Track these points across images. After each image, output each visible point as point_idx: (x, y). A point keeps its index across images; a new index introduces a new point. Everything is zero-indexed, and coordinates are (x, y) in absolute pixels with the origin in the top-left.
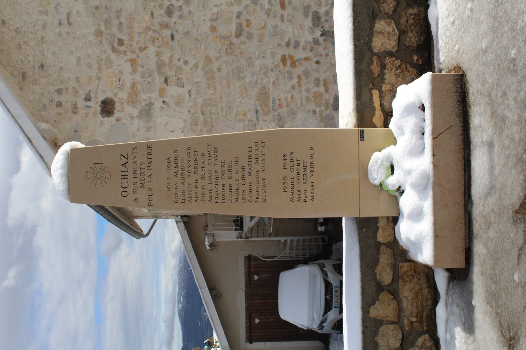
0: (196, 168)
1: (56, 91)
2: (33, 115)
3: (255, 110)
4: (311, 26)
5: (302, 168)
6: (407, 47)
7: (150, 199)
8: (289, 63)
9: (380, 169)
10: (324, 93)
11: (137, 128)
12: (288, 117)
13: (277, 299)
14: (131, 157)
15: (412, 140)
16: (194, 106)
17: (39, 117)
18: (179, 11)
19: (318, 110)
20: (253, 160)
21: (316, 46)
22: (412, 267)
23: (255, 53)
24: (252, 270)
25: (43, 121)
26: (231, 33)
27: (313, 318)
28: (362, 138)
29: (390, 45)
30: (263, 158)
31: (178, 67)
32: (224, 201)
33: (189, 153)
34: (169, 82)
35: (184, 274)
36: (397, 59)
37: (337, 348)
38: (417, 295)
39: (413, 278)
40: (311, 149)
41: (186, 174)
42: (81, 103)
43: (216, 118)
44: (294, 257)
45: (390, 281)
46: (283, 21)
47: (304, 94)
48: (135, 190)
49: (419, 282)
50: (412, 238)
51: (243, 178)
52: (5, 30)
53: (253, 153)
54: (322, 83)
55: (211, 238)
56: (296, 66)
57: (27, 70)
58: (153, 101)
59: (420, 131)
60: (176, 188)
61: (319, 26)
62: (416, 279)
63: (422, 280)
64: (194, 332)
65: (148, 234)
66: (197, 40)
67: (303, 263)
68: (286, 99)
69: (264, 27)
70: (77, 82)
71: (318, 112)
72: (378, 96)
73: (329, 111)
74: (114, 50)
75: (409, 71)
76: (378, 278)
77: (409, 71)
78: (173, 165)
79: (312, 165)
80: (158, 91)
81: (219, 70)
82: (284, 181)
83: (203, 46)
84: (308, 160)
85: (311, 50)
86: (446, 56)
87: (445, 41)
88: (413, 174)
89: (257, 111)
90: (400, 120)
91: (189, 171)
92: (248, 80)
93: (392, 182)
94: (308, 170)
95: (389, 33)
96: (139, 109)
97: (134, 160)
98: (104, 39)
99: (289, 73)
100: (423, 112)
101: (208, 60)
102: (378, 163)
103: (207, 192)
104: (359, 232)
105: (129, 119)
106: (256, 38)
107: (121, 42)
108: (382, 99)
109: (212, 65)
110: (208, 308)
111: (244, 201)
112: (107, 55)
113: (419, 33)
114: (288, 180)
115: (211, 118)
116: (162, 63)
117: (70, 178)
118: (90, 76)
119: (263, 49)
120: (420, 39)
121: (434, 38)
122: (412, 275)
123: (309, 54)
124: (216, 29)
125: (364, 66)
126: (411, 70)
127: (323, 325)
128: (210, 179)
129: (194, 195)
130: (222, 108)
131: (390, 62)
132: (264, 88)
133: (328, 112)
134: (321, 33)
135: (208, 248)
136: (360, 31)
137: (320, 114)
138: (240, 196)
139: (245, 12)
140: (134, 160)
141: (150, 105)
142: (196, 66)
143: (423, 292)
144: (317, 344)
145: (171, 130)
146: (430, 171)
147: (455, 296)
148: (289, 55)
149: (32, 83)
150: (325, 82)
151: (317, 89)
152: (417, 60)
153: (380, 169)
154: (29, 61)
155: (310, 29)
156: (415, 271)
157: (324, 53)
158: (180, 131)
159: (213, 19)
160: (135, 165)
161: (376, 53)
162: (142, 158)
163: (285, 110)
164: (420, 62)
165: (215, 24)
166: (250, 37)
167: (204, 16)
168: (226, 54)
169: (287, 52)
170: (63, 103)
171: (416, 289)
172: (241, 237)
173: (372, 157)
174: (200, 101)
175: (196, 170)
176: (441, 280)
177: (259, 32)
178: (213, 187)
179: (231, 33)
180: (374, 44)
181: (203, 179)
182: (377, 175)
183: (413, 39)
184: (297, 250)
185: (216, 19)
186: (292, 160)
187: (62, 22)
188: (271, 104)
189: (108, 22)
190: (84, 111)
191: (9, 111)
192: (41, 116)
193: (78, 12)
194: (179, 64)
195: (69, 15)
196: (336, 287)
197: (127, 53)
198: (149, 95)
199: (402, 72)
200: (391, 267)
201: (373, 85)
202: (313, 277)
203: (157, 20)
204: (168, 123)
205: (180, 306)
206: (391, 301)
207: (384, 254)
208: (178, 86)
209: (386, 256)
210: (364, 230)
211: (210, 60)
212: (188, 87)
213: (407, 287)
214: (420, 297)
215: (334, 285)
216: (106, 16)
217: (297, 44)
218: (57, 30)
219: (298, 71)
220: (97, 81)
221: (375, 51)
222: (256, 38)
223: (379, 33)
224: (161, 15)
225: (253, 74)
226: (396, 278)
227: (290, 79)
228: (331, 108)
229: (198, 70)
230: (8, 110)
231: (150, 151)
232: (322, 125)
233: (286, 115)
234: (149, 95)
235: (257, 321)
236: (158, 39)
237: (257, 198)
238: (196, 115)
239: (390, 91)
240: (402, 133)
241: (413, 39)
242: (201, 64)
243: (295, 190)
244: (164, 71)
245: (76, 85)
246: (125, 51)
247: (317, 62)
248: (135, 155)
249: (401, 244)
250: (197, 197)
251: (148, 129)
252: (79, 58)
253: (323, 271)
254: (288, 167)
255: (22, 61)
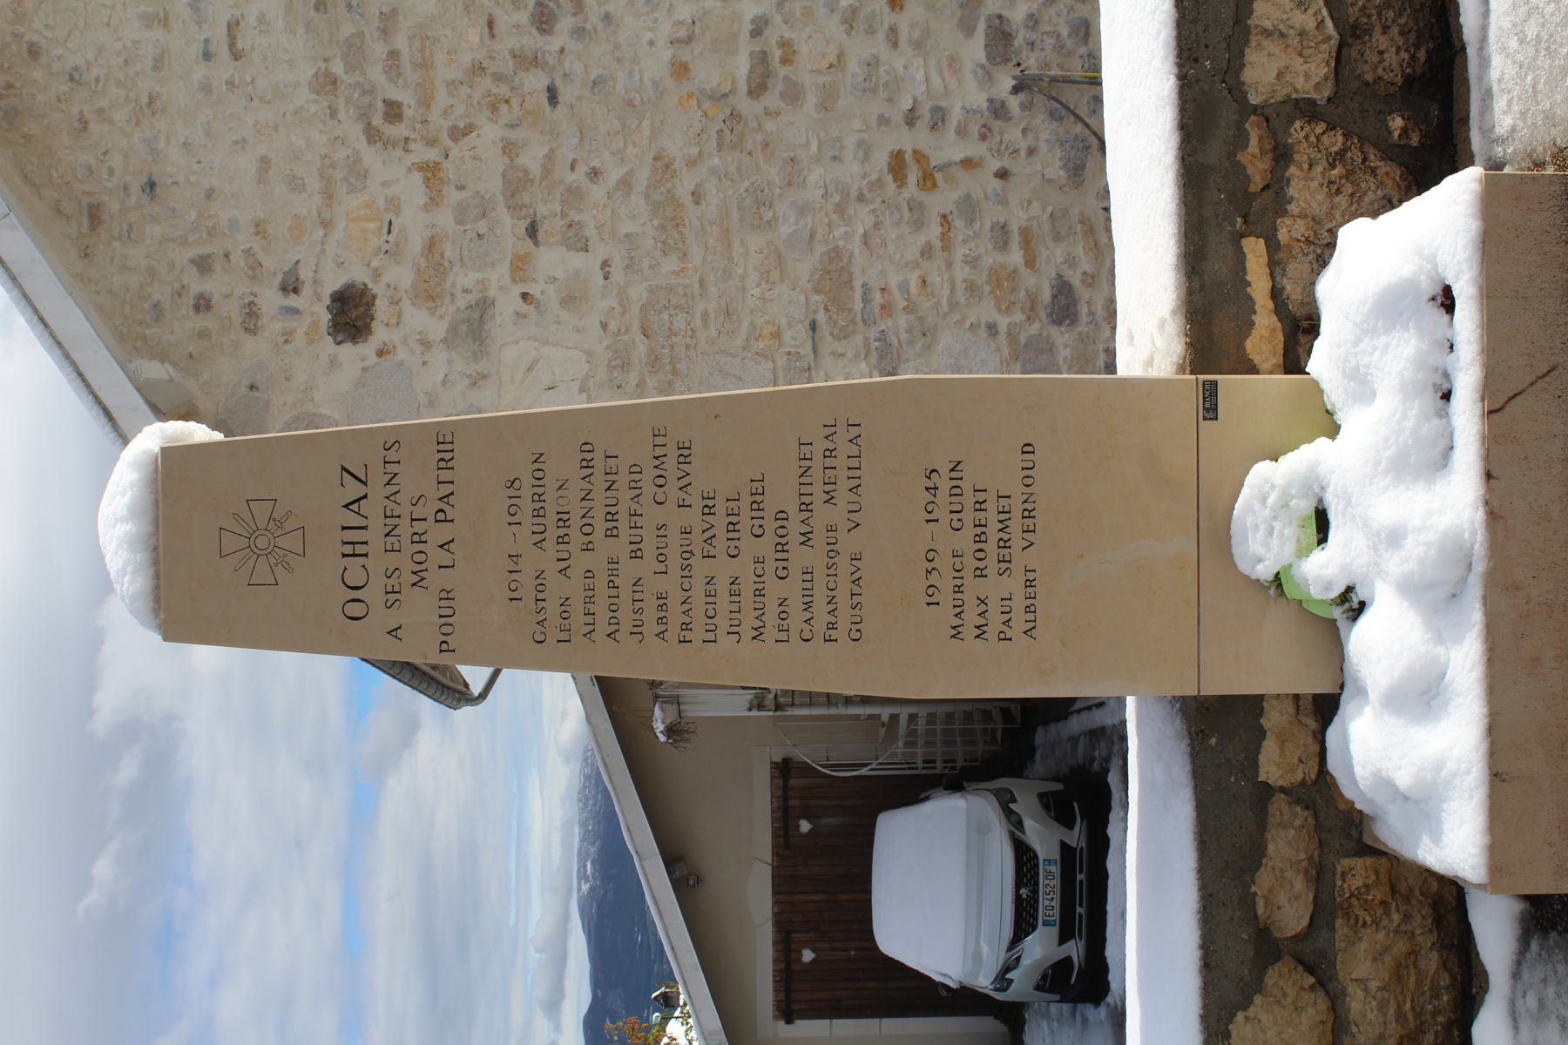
0: (611, 517)
1: (193, 261)
2: (122, 337)
3: (807, 324)
4: (984, 61)
5: (992, 517)
6: (1367, 84)
7: (446, 629)
8: (913, 176)
9: (1277, 525)
10: (1022, 269)
11: (441, 376)
12: (911, 343)
13: (870, 892)
14: (377, 478)
15: (1404, 417)
16: (618, 309)
17: (139, 344)
18: (575, 14)
19: (1003, 322)
20: (818, 490)
21: (997, 125)
22: (1382, 872)
23: (808, 144)
24: (792, 803)
25: (152, 357)
26: (733, 82)
27: (977, 956)
28: (1210, 404)
29: (1307, 76)
30: (856, 482)
31: (568, 190)
32: (711, 636)
33: (587, 465)
34: (540, 235)
35: (595, 796)
36: (1331, 127)
37: (1048, 1040)
38: (1398, 973)
39: (1387, 913)
40: (1027, 449)
41: (576, 539)
42: (270, 299)
43: (688, 347)
44: (920, 765)
45: (1305, 922)
46: (895, 44)
47: (961, 273)
48: (393, 597)
49: (1409, 928)
50: (1403, 779)
51: (780, 556)
52: (38, 75)
53: (818, 463)
54: (1015, 239)
55: (672, 708)
56: (935, 186)
57: (105, 198)
58: (491, 293)
59: (1436, 387)
60: (540, 587)
61: (1007, 60)
62: (1396, 917)
63: (1418, 919)
64: (626, 993)
65: (483, 695)
66: (630, 103)
67: (946, 789)
68: (904, 287)
69: (838, 64)
70: (258, 233)
71: (1003, 328)
72: (1265, 259)
73: (1037, 325)
74: (372, 135)
75: (1373, 171)
76: (1260, 911)
77: (1373, 171)
78: (527, 506)
79: (1029, 506)
80: (507, 264)
81: (697, 197)
82: (930, 566)
83: (646, 123)
84: (1016, 490)
85: (983, 137)
86: (1523, 114)
87: (1520, 57)
88: (1409, 543)
89: (814, 326)
90: (1356, 343)
91: (587, 529)
92: (785, 230)
93: (1321, 570)
94: (1015, 525)
95: (1302, 34)
96: (448, 318)
97: (390, 489)
98: (342, 101)
99: (915, 207)
100: (1446, 317)
101: (663, 166)
102: (1271, 500)
103: (650, 604)
104: (1192, 746)
105: (419, 349)
106: (811, 100)
107: (393, 111)
108: (1278, 270)
109: (676, 181)
110: (661, 918)
111: (783, 636)
112: (350, 151)
113: (1412, 36)
114: (944, 563)
115: (672, 347)
116: (521, 175)
117: (161, 550)
118: (296, 216)
119: (835, 134)
120: (1413, 57)
121: (1471, 51)
122: (1382, 902)
123: (976, 149)
124: (687, 69)
125: (1214, 153)
126: (1383, 167)
127: (1008, 976)
128: (661, 558)
129: (602, 616)
130: (705, 316)
131: (1307, 137)
132: (835, 253)
133: (1034, 329)
134: (1014, 82)
135: (662, 738)
136: (1200, 28)
137: (1009, 334)
138: (771, 618)
139: (778, 18)
140: (390, 489)
141: (483, 306)
142: (625, 184)
143: (1422, 964)
144: (988, 1025)
145: (547, 382)
146: (1474, 534)
147: (1551, 991)
148: (914, 151)
149: (120, 237)
150: (1025, 233)
151: (1001, 258)
152: (1404, 132)
153: (1277, 525)
154: (111, 171)
155: (980, 72)
156: (1393, 890)
157: (1023, 146)
158: (575, 386)
159: (679, 41)
160: (391, 505)
161: (1256, 107)
162: (417, 479)
163: (903, 321)
164: (1415, 140)
165: (685, 55)
166: (793, 95)
167: (651, 30)
168: (720, 148)
169: (906, 141)
170: (214, 302)
171: (1395, 951)
172: (760, 707)
173: (1250, 480)
174: (638, 292)
175: (610, 525)
176: (1494, 930)
177: (821, 80)
178: (670, 585)
179: (733, 82)
180: (1248, 75)
181: (635, 555)
182: (1266, 545)
183: (1387, 54)
184: (928, 744)
185: (690, 39)
186: (956, 490)
187: (212, 48)
188: (858, 305)
189: (354, 51)
190: (279, 326)
191: (46, 325)
192: (145, 339)
193: (262, 19)
194: (571, 177)
195: (233, 27)
196: (1048, 862)
197: (412, 146)
198: (479, 276)
199: (1348, 175)
200: (1307, 873)
201: (1245, 222)
202: (979, 830)
203: (507, 43)
204: (536, 362)
205: (585, 887)
206: (1307, 997)
207: (1283, 826)
208: (569, 249)
209: (1292, 833)
210: (1213, 741)
211: (668, 166)
212: (600, 251)
213: (1363, 946)
214: (1412, 979)
215: (1041, 855)
216: (347, 30)
217: (939, 118)
218: (197, 76)
219: (942, 200)
220: (321, 233)
221: (1254, 99)
222: (811, 100)
223: (1267, 34)
224: (517, 26)
225: (803, 209)
226: (1324, 912)
227: (919, 225)
228: (1043, 316)
229: (633, 198)
230: (42, 319)
231: (447, 456)
232: (1018, 366)
233: (904, 336)
234: (479, 276)
235: (808, 956)
236: (507, 102)
237: (832, 626)
238: (625, 338)
239: (1308, 241)
240: (1364, 390)
241: (1391, 58)
242: (642, 177)
243: (969, 597)
244: (527, 199)
245: (256, 244)
246: (407, 139)
247: (1002, 174)
248: (392, 468)
249: (1348, 793)
250: (614, 620)
251: (478, 380)
252: (265, 161)
253: (1009, 814)
254: (942, 513)
255: (90, 169)
